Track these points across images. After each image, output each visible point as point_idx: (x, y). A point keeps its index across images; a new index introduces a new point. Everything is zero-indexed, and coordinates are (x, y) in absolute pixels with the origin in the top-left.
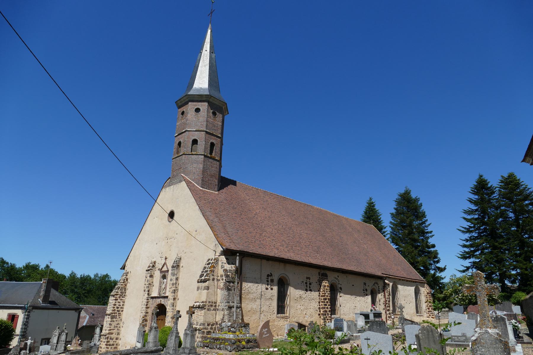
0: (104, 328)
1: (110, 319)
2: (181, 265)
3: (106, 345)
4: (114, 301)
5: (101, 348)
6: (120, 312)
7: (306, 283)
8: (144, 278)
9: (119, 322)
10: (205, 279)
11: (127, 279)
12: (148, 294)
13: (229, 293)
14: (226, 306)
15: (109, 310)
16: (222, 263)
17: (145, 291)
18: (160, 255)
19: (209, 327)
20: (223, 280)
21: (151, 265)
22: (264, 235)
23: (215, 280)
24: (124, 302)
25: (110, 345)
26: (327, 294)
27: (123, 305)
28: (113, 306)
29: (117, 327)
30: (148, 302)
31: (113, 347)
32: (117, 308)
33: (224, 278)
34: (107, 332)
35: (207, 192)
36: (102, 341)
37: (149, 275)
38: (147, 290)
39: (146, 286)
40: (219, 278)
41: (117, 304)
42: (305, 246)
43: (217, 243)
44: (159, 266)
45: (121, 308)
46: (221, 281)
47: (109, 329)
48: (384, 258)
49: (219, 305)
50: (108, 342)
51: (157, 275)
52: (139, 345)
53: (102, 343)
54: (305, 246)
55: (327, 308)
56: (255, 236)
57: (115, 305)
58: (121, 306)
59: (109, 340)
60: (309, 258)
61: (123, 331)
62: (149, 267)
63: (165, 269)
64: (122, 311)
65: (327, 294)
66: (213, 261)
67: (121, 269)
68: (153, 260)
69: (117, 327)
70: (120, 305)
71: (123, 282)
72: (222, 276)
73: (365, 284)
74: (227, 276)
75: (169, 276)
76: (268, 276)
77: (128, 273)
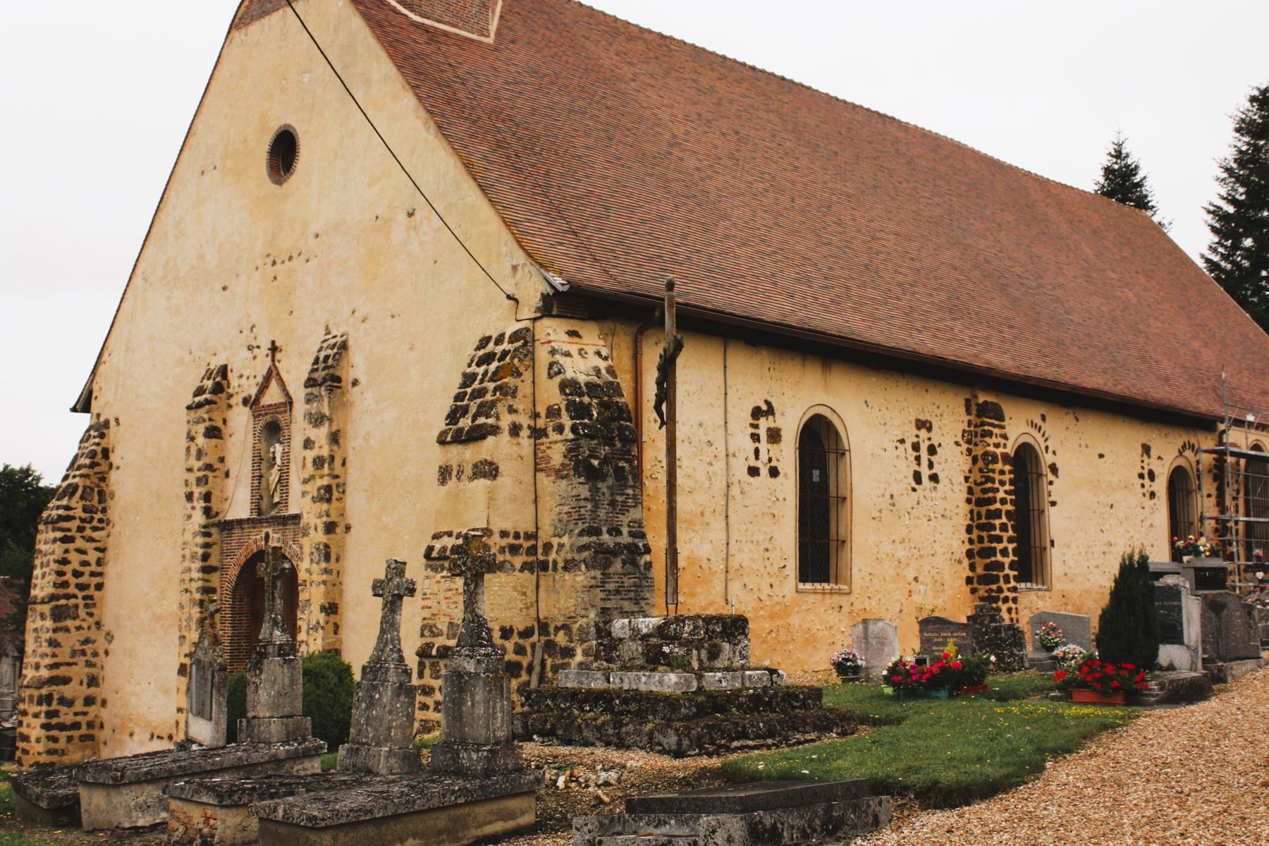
0: (29, 659)
1: (49, 623)
2: (348, 375)
3: (45, 727)
4: (59, 548)
5: (26, 738)
6: (92, 591)
7: (916, 447)
8: (184, 442)
9: (93, 634)
10: (472, 429)
11: (106, 453)
12: (207, 511)
13: (594, 490)
14: (582, 548)
15: (42, 585)
16: (553, 352)
17: (189, 497)
18: (247, 338)
19: (510, 645)
20: (560, 429)
21: (209, 384)
22: (720, 232)
23: (525, 433)
24: (103, 550)
25: (62, 727)
26: (1001, 495)
27: (99, 562)
28: (54, 566)
29: (83, 653)
30: (206, 545)
31: (76, 733)
32: (77, 574)
33: (567, 421)
34: (45, 673)
35: (446, 34)
36: (25, 713)
37: (201, 428)
38: (198, 491)
39: (192, 477)
40: (541, 423)
41: (75, 558)
42: (900, 285)
43: (520, 258)
44: (243, 384)
45: (93, 574)
46: (554, 436)
47: (47, 661)
48: (1206, 345)
49: (548, 547)
50: (50, 714)
51: (240, 422)
52: (204, 731)
53: (26, 720)
54: (900, 285)
55: (1004, 552)
56: (684, 236)
57: (64, 562)
58: (94, 568)
59: (55, 706)
60: (925, 336)
61: (114, 670)
62: (200, 391)
63: (273, 396)
64: (99, 587)
65: (1001, 495)
66: (505, 346)
67: (74, 410)
68: (216, 363)
69: (89, 653)
70: (85, 564)
71: (93, 465)
72: (553, 412)
73: (1146, 449)
74: (578, 411)
75: (299, 428)
76: (757, 413)
77: (106, 424)
